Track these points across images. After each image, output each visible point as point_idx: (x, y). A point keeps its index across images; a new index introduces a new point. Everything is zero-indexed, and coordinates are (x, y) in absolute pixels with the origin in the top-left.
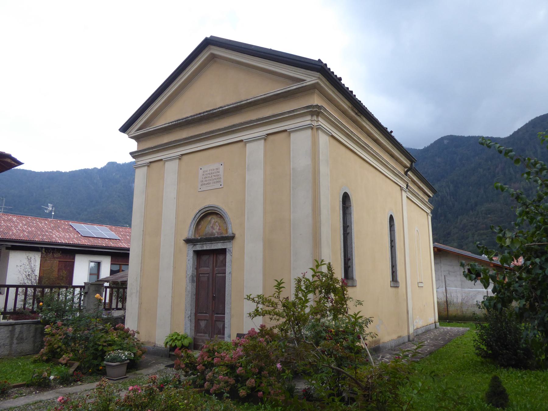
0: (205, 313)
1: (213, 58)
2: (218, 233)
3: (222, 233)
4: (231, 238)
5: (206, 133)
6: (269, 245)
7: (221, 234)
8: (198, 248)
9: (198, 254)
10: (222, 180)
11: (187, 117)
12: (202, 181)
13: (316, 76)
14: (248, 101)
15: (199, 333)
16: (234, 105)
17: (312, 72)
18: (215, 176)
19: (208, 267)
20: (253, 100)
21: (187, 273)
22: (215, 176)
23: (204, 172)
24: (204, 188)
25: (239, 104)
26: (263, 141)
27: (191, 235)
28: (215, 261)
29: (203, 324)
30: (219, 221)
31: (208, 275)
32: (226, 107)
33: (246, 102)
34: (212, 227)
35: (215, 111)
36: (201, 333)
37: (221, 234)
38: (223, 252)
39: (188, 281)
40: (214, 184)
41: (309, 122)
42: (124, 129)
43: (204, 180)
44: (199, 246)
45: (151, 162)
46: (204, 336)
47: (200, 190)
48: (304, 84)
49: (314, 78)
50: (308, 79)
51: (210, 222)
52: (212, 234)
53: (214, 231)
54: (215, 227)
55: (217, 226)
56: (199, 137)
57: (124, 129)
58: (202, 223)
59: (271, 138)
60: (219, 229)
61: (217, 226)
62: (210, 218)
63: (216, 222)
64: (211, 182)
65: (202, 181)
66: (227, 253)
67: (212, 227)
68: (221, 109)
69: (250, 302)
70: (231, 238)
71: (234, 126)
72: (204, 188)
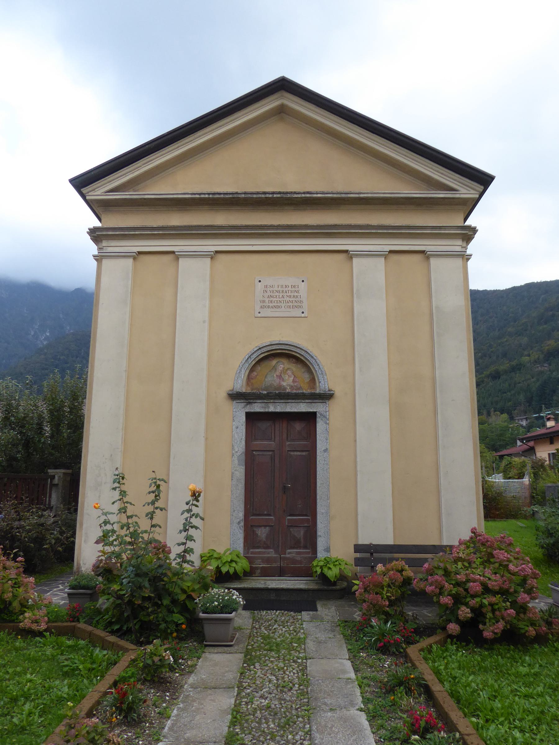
0: (269, 515)
1: (281, 112)
2: (292, 387)
3: (300, 388)
4: (326, 397)
5: (279, 226)
6: (398, 411)
7: (299, 389)
8: (257, 407)
9: (251, 417)
10: (305, 305)
11: (237, 193)
12: (264, 301)
13: (477, 189)
14: (362, 196)
15: (254, 548)
16: (335, 196)
17: (473, 183)
18: (290, 297)
19: (270, 440)
20: (370, 195)
21: (233, 448)
22: (290, 297)
23: (266, 286)
24: (267, 312)
25: (343, 196)
26: (209, 260)
27: (240, 386)
28: (273, 431)
29: (262, 533)
30: (294, 369)
31: (271, 453)
32: (319, 195)
33: (357, 196)
34: (280, 377)
35: (295, 196)
36: (258, 547)
37: (299, 389)
38: (311, 418)
39: (236, 462)
40: (288, 310)
41: (458, 249)
42: (81, 183)
43: (267, 300)
44: (260, 405)
45: (140, 253)
46: (264, 553)
47: (259, 315)
48: (457, 196)
49: (472, 192)
50: (463, 191)
51: (275, 368)
52: (280, 387)
53: (284, 384)
54: (286, 377)
55: (289, 376)
56: (264, 229)
57: (81, 183)
58: (259, 368)
59: (395, 257)
60: (294, 381)
61: (289, 376)
62: (274, 362)
63: (288, 369)
64: (283, 305)
65: (264, 301)
66: (318, 420)
67: (286, 376)
68: (308, 195)
69: (161, 506)
70: (326, 397)
71: (307, 227)
72: (267, 312)
